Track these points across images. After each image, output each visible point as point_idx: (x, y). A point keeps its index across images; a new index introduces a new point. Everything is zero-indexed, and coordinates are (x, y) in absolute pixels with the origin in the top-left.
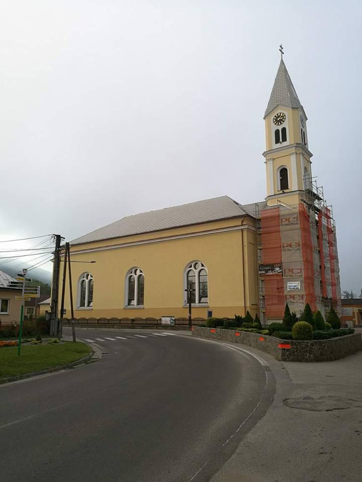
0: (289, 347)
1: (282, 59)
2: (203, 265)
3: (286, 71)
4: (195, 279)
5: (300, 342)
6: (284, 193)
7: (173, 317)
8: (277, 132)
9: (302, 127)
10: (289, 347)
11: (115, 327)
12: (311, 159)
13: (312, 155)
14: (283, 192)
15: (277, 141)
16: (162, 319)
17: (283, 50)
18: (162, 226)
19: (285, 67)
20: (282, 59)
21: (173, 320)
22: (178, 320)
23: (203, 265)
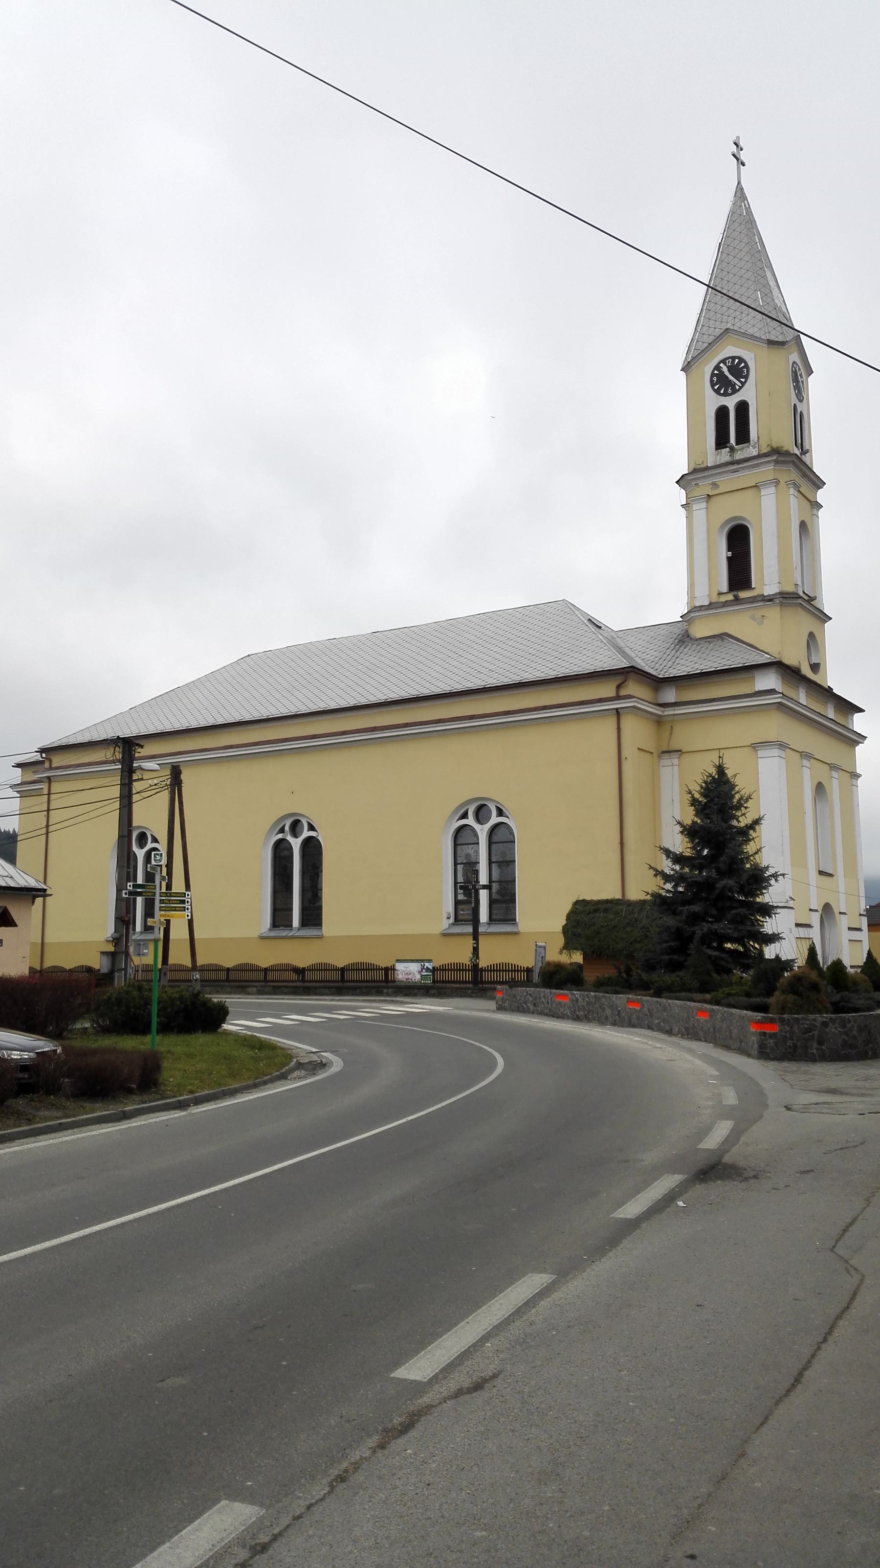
0: (776, 1029)
1: (739, 183)
2: (500, 813)
3: (750, 222)
4: (477, 852)
5: (797, 1019)
6: (737, 599)
7: (430, 961)
8: (722, 414)
9: (794, 400)
10: (776, 1029)
11: (249, 990)
12: (821, 496)
13: (825, 483)
14: (735, 596)
15: (721, 441)
16: (400, 967)
17: (743, 156)
18: (373, 691)
19: (748, 209)
20: (739, 183)
21: (428, 969)
22: (443, 969)
23: (500, 813)
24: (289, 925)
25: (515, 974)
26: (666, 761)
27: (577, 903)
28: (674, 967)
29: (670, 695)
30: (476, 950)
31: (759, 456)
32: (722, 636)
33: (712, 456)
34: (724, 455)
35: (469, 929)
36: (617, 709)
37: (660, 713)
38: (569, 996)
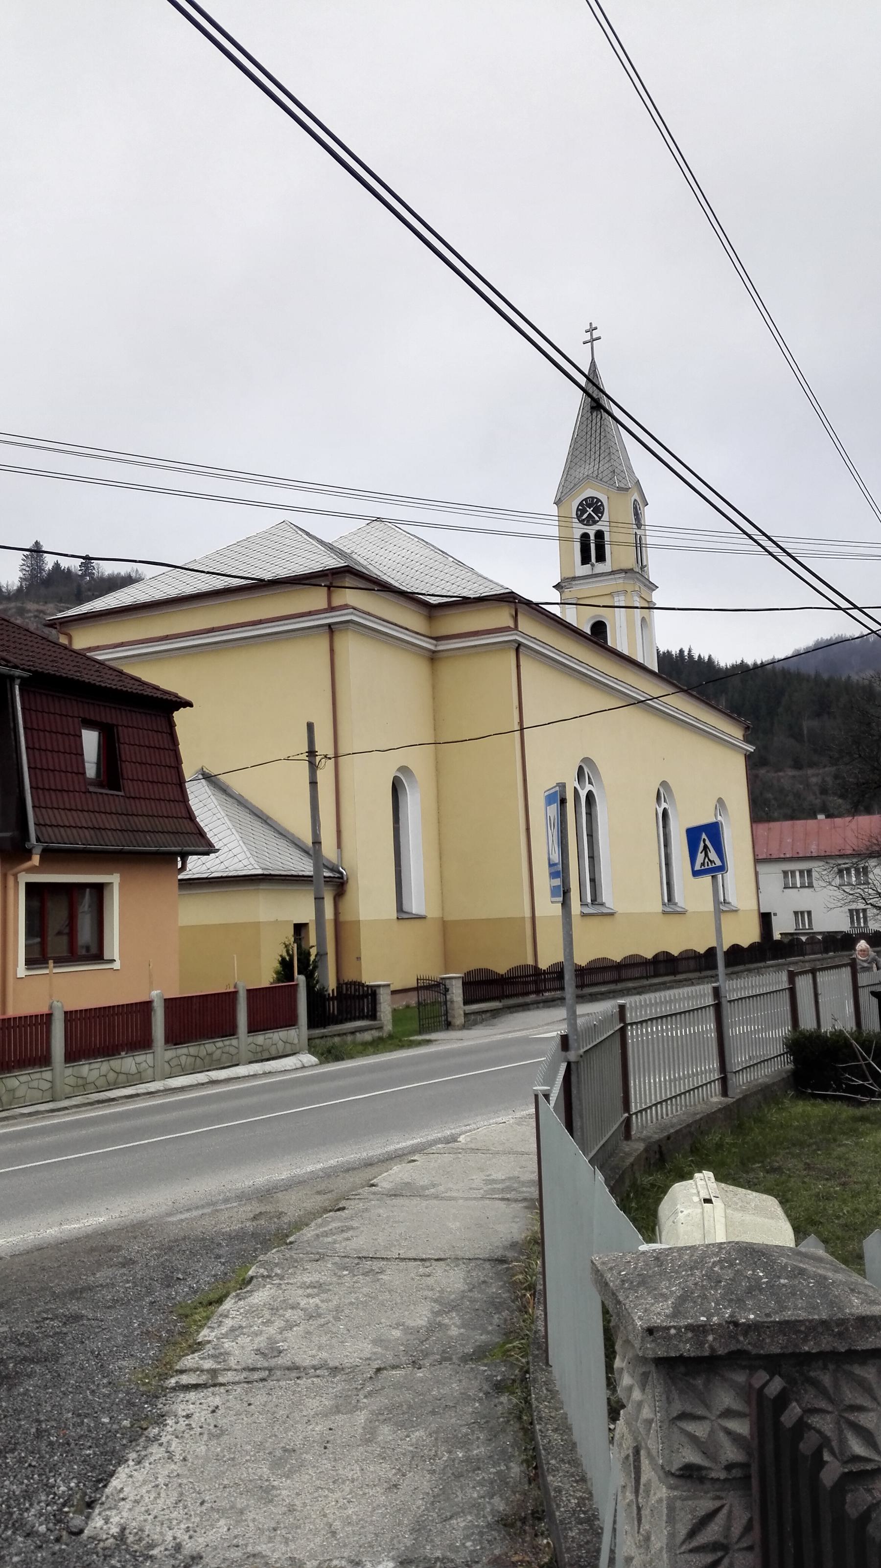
1: (593, 359)
15: (585, 559)
20: (593, 359)
25: (118, 1018)
27: (733, 946)
34: (586, 570)
36: (329, 626)
37: (432, 647)
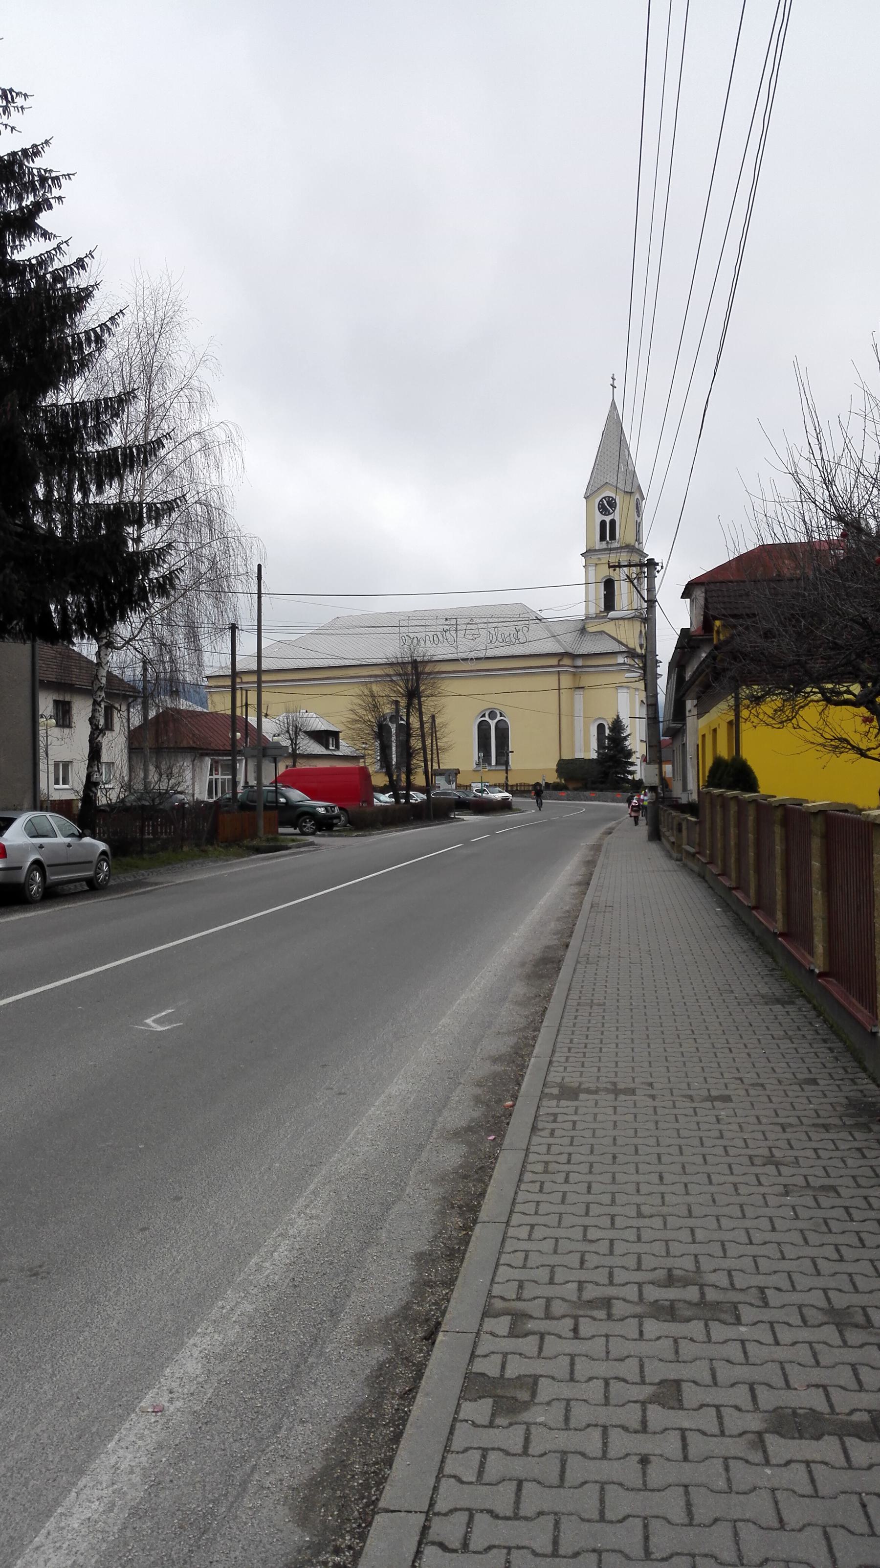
2: (501, 715)
8: (603, 523)
15: (603, 538)
16: (473, 785)
24: (490, 764)
26: (578, 692)
28: (602, 783)
29: (579, 662)
30: (507, 778)
31: (621, 548)
32: (602, 632)
33: (599, 545)
34: (604, 545)
35: (504, 768)
38: (564, 793)
